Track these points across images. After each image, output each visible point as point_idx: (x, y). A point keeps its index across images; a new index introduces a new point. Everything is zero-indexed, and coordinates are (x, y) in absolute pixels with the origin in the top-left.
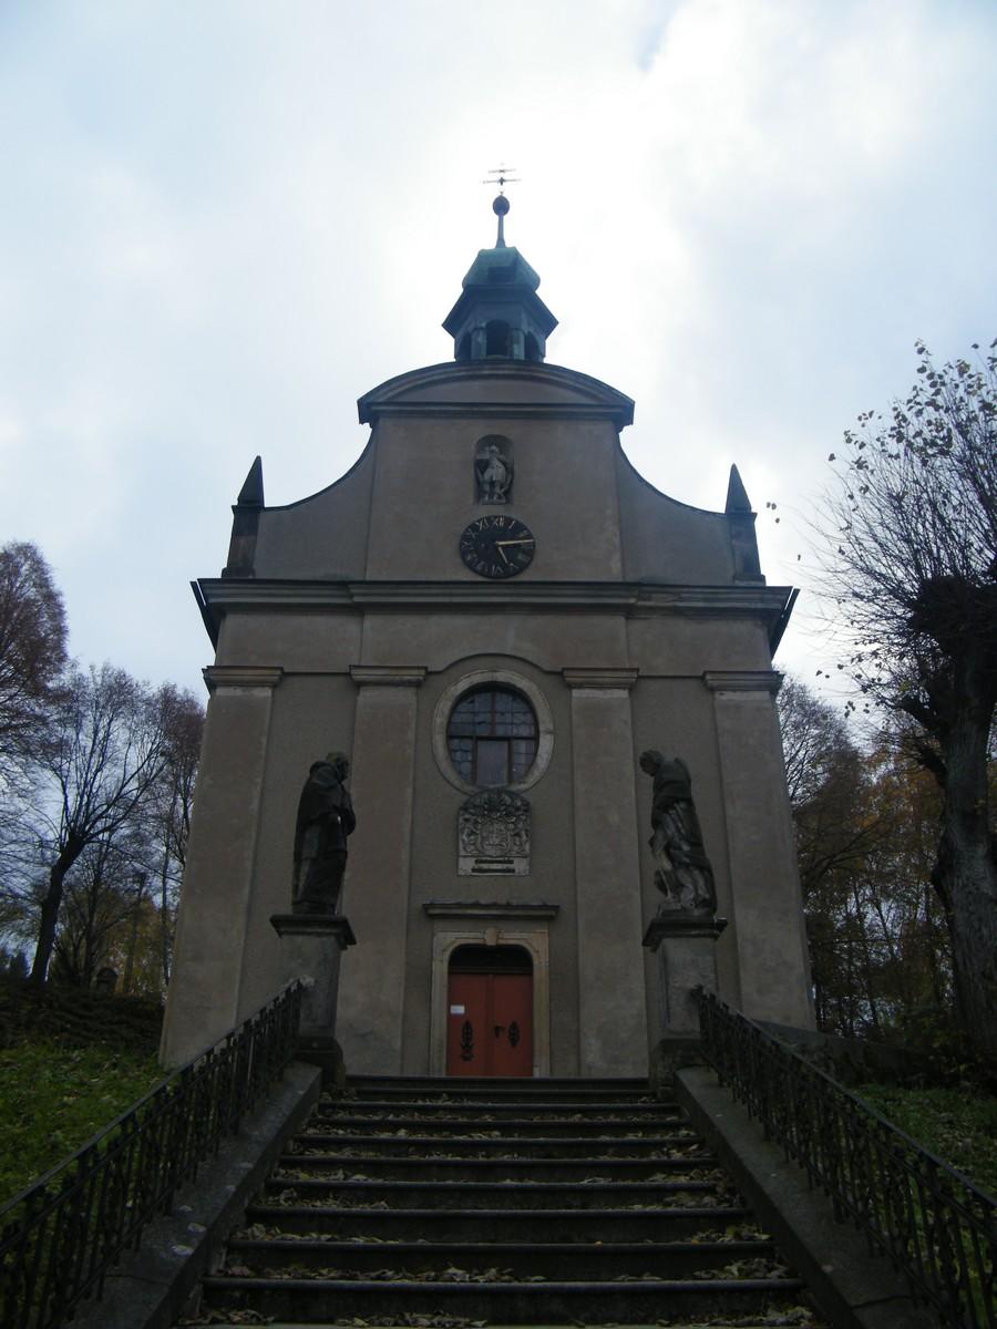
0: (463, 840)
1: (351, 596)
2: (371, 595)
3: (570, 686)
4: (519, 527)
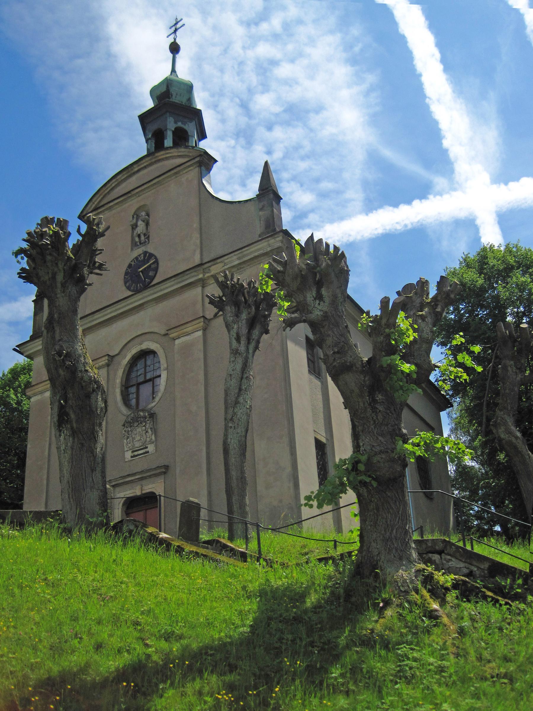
2: (157, 292)
3: (174, 339)
4: (151, 255)
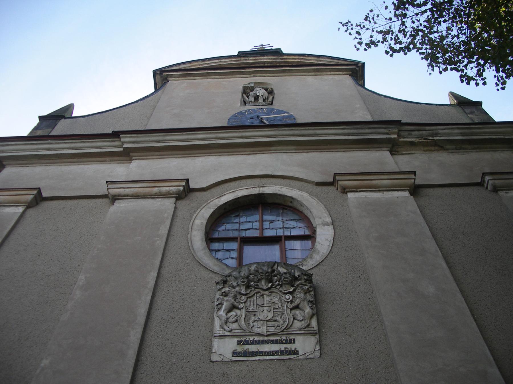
1: (123, 143)
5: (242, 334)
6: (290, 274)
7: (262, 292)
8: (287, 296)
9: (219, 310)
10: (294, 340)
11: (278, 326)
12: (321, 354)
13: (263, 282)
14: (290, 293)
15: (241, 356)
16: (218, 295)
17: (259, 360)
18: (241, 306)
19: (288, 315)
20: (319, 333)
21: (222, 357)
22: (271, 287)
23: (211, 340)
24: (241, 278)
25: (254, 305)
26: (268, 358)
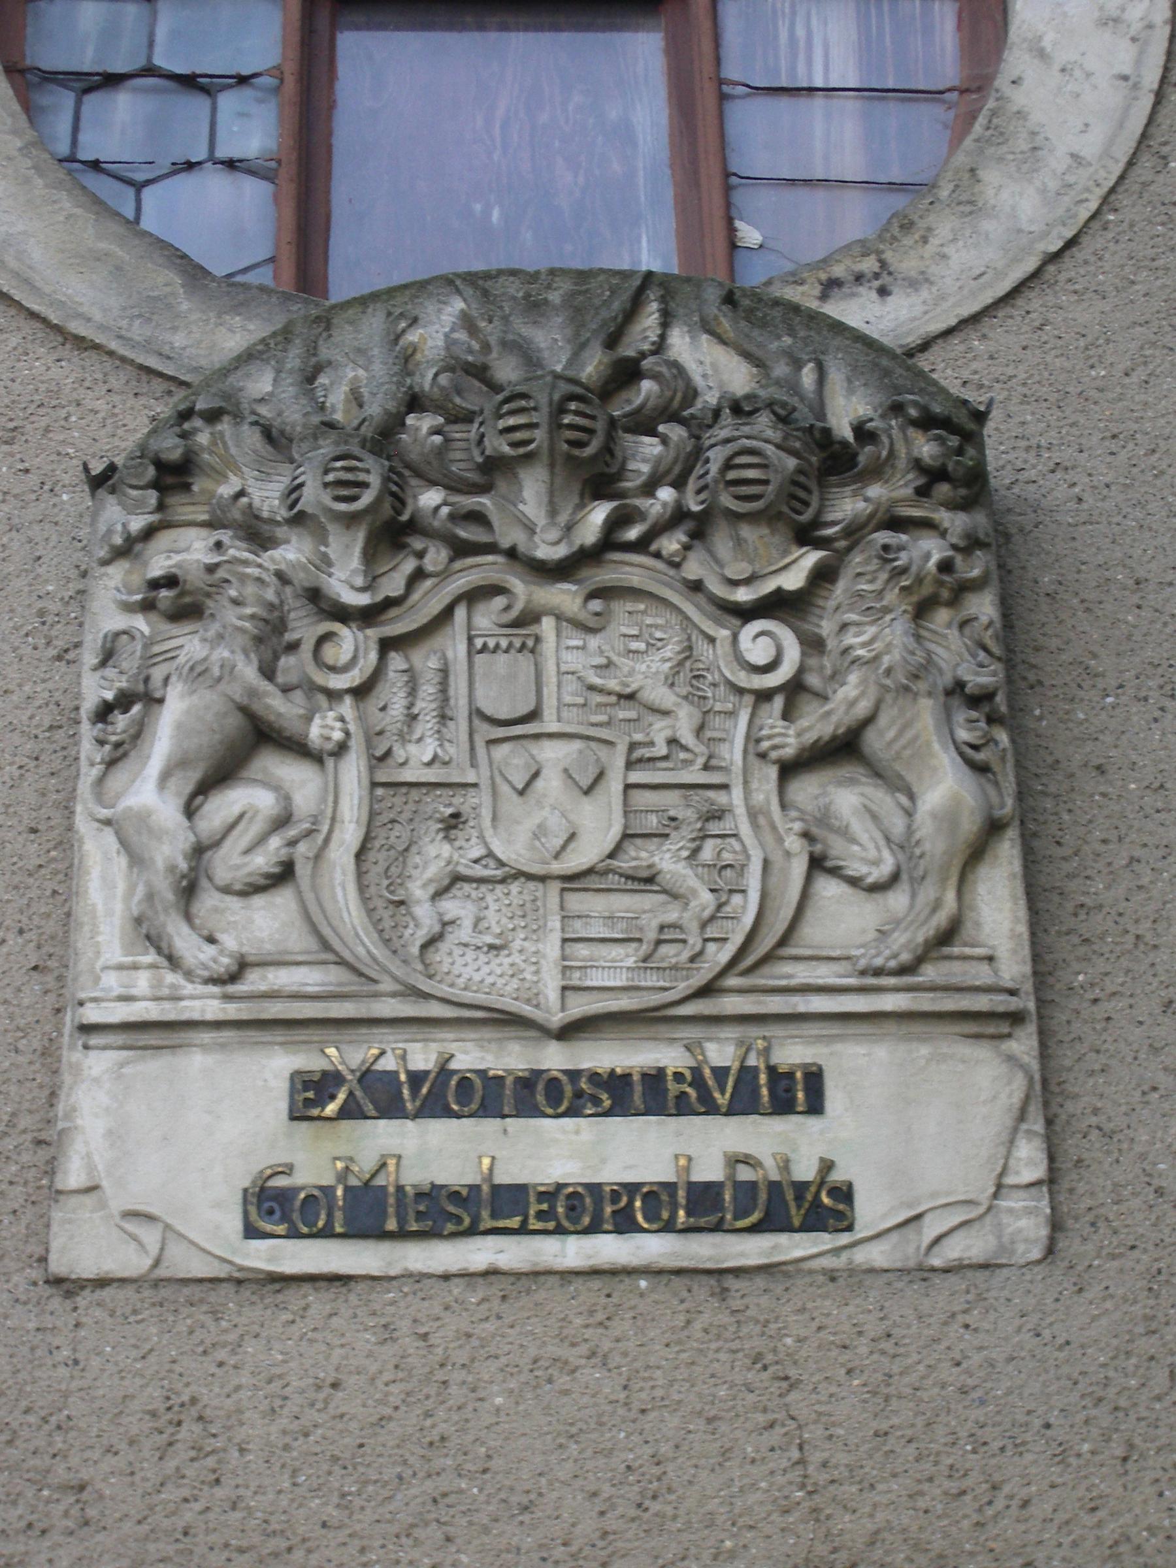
0: (130, 837)
5: (346, 1010)
6: (784, 419)
7: (518, 586)
8: (756, 642)
9: (118, 755)
10: (814, 1079)
11: (668, 934)
12: (1056, 1225)
13: (532, 491)
14: (779, 605)
15: (326, 1233)
16: (109, 610)
17: (491, 1273)
18: (323, 728)
19: (760, 826)
20: (1035, 1015)
21: (151, 1236)
22: (609, 543)
23: (49, 1053)
24: (327, 448)
25: (444, 718)
26: (574, 1251)
